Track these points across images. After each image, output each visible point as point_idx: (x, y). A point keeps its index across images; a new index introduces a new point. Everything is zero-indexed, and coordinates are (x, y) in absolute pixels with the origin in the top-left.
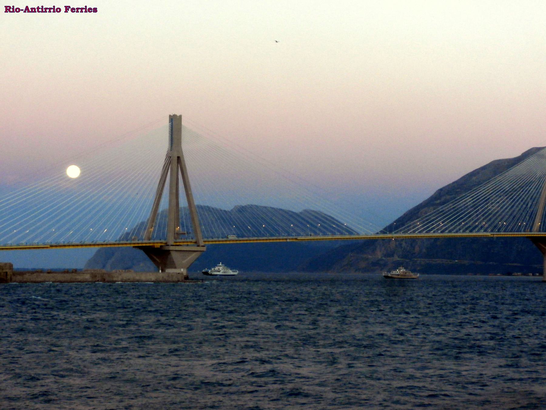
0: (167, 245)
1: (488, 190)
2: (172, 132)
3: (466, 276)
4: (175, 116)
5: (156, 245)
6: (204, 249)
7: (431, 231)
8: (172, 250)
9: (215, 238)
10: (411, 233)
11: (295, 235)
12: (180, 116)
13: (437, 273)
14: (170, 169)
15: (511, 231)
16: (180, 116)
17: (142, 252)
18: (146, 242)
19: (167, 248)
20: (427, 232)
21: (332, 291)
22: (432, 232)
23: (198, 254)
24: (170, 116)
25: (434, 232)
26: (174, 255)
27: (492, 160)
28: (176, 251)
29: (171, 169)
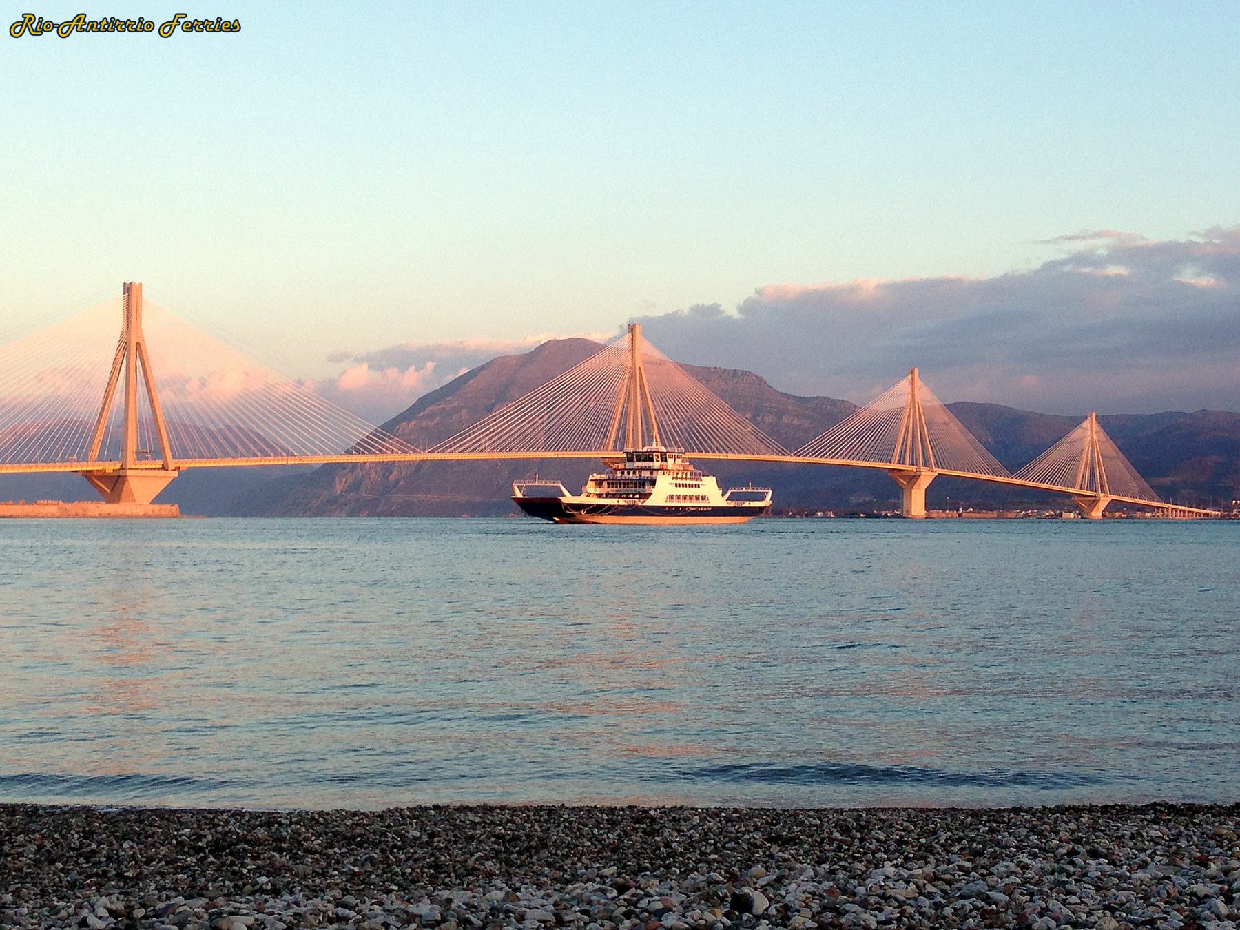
16: (140, 284)
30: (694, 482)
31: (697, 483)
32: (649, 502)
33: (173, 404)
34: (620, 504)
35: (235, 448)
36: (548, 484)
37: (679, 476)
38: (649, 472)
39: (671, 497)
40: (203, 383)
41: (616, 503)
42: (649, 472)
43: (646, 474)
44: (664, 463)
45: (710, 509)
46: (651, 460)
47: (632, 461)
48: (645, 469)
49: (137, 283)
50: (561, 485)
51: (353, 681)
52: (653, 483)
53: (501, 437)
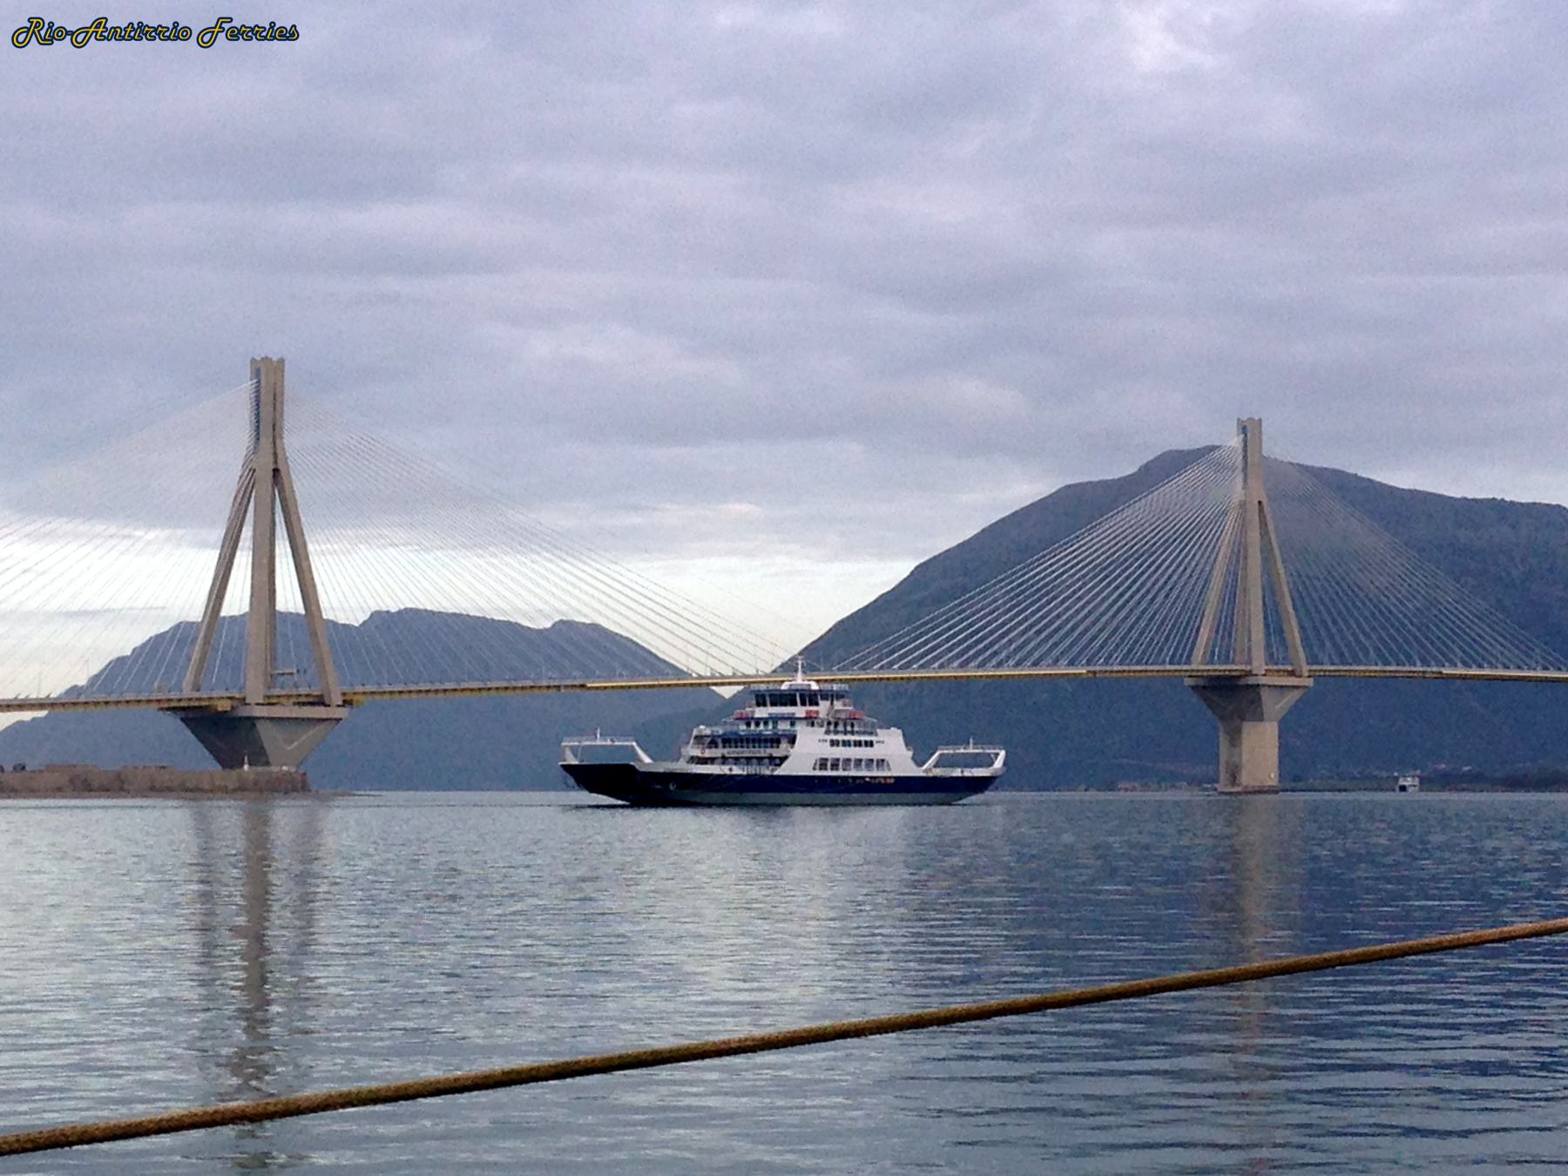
0: (243, 701)
1: (1115, 538)
2: (257, 405)
3: (1018, 794)
4: (266, 359)
5: (214, 703)
6: (1310, 682)
7: (934, 663)
8: (1264, 685)
9: (450, 681)
10: (882, 668)
11: (580, 677)
12: (281, 361)
13: (1144, 776)
14: (252, 499)
15: (1138, 663)
16: (281, 361)
17: (174, 723)
18: (186, 692)
19: (244, 712)
20: (962, 666)
21: (1376, 811)
22: (936, 665)
23: (1296, 694)
24: (253, 361)
25: (941, 666)
26: (266, 733)
27: (1167, 448)
28: (271, 719)
29: (281, 501)
30: (863, 738)
31: (868, 738)
32: (782, 771)
33: (1246, 920)
34: (734, 772)
35: (1342, 655)
36: (616, 743)
37: (841, 728)
38: (789, 722)
39: (823, 764)
40: (864, 952)
41: (728, 772)
42: (789, 722)
43: (783, 726)
44: (814, 708)
45: (892, 781)
46: (794, 704)
47: (765, 705)
48: (783, 718)
49: (275, 359)
50: (634, 744)
51: (479, 970)
52: (792, 740)
53: (1069, 562)
